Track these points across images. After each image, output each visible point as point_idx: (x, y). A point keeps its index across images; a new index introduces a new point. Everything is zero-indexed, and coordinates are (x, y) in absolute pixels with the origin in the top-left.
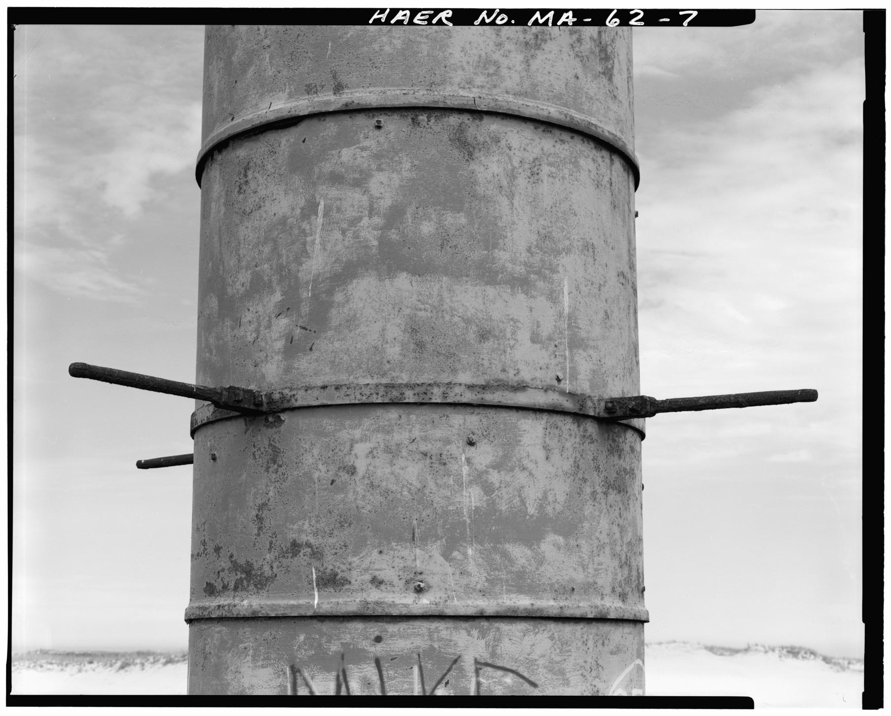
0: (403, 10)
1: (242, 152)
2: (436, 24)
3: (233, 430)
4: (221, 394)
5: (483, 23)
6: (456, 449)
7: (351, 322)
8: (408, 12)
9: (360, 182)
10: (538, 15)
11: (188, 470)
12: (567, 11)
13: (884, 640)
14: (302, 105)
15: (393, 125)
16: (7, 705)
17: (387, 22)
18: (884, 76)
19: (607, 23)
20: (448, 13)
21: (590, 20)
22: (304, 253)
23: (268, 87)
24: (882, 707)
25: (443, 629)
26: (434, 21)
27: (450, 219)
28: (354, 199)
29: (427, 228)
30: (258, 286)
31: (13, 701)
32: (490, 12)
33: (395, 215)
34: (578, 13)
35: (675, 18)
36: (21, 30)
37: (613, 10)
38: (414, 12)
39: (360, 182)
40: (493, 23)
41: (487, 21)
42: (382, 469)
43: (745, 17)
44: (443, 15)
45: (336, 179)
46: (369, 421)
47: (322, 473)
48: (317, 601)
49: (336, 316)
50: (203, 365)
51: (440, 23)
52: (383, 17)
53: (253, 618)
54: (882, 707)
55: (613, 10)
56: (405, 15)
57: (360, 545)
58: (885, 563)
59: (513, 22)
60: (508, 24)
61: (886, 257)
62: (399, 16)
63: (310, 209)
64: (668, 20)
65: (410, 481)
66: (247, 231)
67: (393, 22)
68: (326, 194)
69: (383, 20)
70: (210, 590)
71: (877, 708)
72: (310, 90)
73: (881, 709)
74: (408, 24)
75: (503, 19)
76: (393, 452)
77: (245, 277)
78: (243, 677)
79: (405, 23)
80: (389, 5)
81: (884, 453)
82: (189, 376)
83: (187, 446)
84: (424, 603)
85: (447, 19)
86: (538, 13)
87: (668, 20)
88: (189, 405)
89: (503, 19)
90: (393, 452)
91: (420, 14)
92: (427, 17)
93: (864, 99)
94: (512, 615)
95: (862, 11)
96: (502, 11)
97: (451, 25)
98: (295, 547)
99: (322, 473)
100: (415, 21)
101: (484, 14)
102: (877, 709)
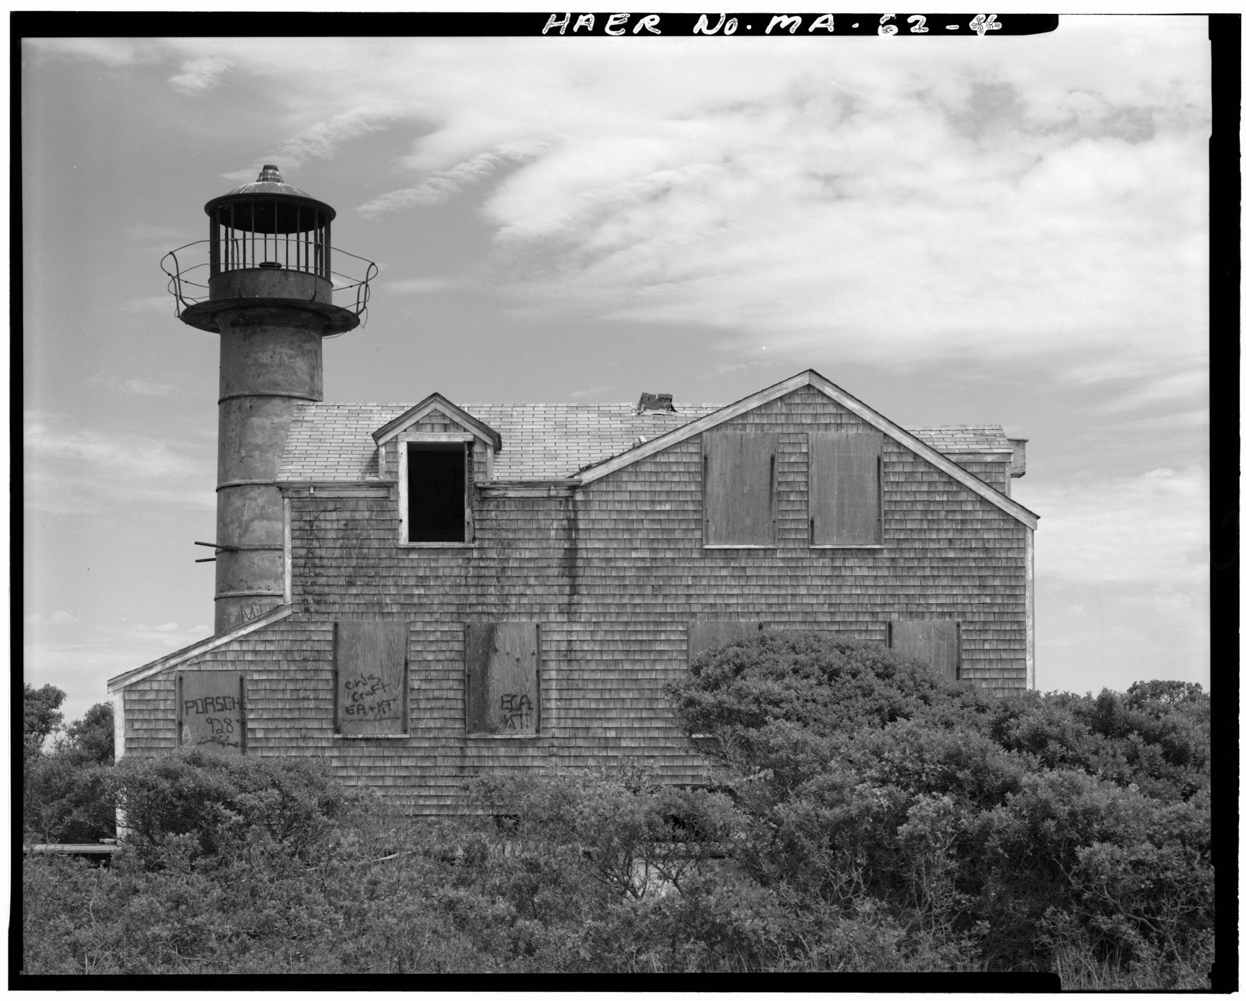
0: (585, 14)
1: (228, 490)
2: (547, 35)
3: (227, 554)
5: (700, 33)
6: (277, 559)
7: (253, 531)
8: (592, 18)
9: (255, 500)
11: (214, 562)
14: (242, 482)
15: (263, 488)
16: (10, 989)
18: (1239, 108)
19: (607, 30)
20: (653, 20)
22: (243, 515)
23: (235, 477)
25: (275, 599)
26: (637, 29)
27: (275, 508)
28: (254, 504)
29: (270, 510)
30: (232, 522)
31: (17, 981)
33: (263, 507)
39: (255, 500)
40: (721, 33)
42: (261, 563)
44: (647, 22)
45: (250, 499)
46: (258, 553)
47: (247, 564)
48: (246, 592)
49: (250, 529)
50: (218, 538)
51: (644, 32)
52: (565, 24)
53: (232, 597)
56: (588, 20)
57: (256, 580)
59: (749, 27)
63: (244, 505)
66: (230, 509)
67: (575, 29)
68: (248, 503)
69: (590, 29)
70: (222, 591)
71: (1229, 992)
72: (244, 478)
76: (263, 559)
77: (229, 519)
80: (568, 10)
82: (214, 542)
83: (214, 557)
84: (270, 592)
88: (214, 549)
90: (263, 559)
95: (1207, 17)
96: (729, 16)
98: (241, 580)
99: (247, 564)
102: (1230, 993)
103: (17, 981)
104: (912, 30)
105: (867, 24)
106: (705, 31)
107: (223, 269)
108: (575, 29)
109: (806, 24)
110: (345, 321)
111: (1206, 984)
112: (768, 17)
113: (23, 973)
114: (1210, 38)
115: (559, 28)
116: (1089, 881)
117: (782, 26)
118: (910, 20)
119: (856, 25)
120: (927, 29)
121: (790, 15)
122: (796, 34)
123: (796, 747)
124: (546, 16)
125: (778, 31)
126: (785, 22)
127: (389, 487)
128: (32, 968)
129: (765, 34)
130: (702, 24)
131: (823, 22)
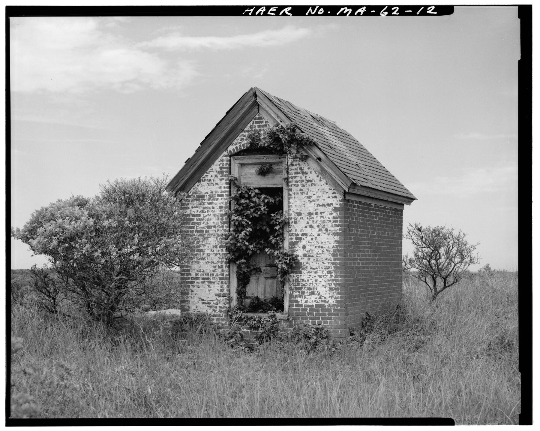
0: (343, 7)
2: (357, 15)
4: (296, 259)
5: (310, 14)
8: (264, 8)
10: (310, 9)
12: (361, 7)
16: (6, 426)
19: (381, 14)
21: (372, 12)
31: (10, 422)
32: (313, 7)
35: (423, 11)
36: (12, 19)
38: (268, 8)
40: (316, 14)
41: (313, 13)
44: (286, 10)
51: (284, 14)
60: (324, 14)
64: (411, 11)
67: (257, 13)
75: (321, 12)
78: (31, 394)
79: (361, 14)
85: (288, 12)
86: (311, 8)
87: (411, 11)
88: (458, 235)
89: (321, 12)
91: (272, 8)
92: (275, 10)
93: (519, 58)
94: (358, 416)
95: (517, 7)
96: (320, 7)
97: (291, 15)
100: (269, 13)
101: (310, 9)
103: (10, 422)
104: (393, 13)
108: (257, 13)
111: (517, 420)
112: (339, 7)
113: (10, 418)
114: (519, 18)
119: (374, 11)
120: (398, 14)
122: (263, 15)
123: (155, 316)
128: (13, 416)
130: (362, 10)
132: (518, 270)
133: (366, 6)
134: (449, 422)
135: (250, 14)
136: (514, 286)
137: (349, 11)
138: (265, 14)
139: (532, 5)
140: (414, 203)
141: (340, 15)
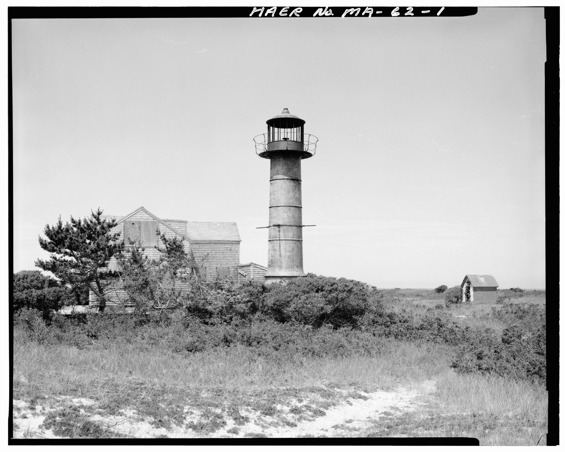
0: (349, 8)
5: (317, 16)
13: (559, 402)
16: (9, 444)
17: (360, 15)
18: (559, 48)
24: (558, 444)
31: (12, 442)
34: (376, 9)
36: (13, 20)
37: (441, 7)
43: (472, 11)
54: (558, 444)
55: (441, 7)
58: (560, 354)
61: (560, 162)
62: (269, 11)
64: (381, 12)
65: (140, 381)
67: (363, 14)
71: (555, 445)
73: (557, 446)
74: (275, 16)
79: (273, 15)
81: (559, 404)
87: (381, 12)
93: (546, 61)
95: (544, 8)
100: (280, 14)
102: (555, 446)
103: (12, 442)
104: (406, 14)
105: (386, 12)
106: (320, 15)
107: (300, 127)
108: (266, 15)
109: (362, 12)
110: (308, 155)
111: (544, 439)
114: (545, 18)
115: (369, 14)
116: (38, 369)
117: (351, 13)
118: (408, 9)
120: (413, 14)
121: (355, 8)
122: (357, 16)
124: (252, 8)
125: (256, 15)
126: (352, 11)
127: (186, 223)
128: (18, 435)
129: (313, 17)
130: (394, 13)
131: (357, 11)
132: (545, 290)
133: (256, 7)
134: (474, 442)
135: (260, 15)
136: (541, 302)
137: (357, 11)
138: (277, 15)
139: (559, 7)
140: (324, 417)
141: (253, 16)
